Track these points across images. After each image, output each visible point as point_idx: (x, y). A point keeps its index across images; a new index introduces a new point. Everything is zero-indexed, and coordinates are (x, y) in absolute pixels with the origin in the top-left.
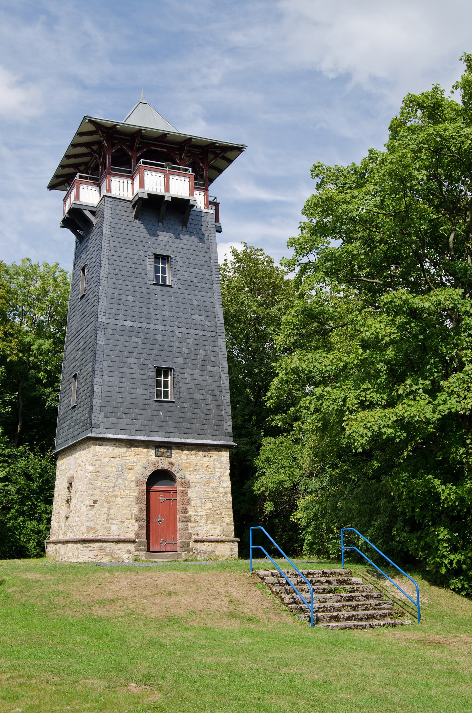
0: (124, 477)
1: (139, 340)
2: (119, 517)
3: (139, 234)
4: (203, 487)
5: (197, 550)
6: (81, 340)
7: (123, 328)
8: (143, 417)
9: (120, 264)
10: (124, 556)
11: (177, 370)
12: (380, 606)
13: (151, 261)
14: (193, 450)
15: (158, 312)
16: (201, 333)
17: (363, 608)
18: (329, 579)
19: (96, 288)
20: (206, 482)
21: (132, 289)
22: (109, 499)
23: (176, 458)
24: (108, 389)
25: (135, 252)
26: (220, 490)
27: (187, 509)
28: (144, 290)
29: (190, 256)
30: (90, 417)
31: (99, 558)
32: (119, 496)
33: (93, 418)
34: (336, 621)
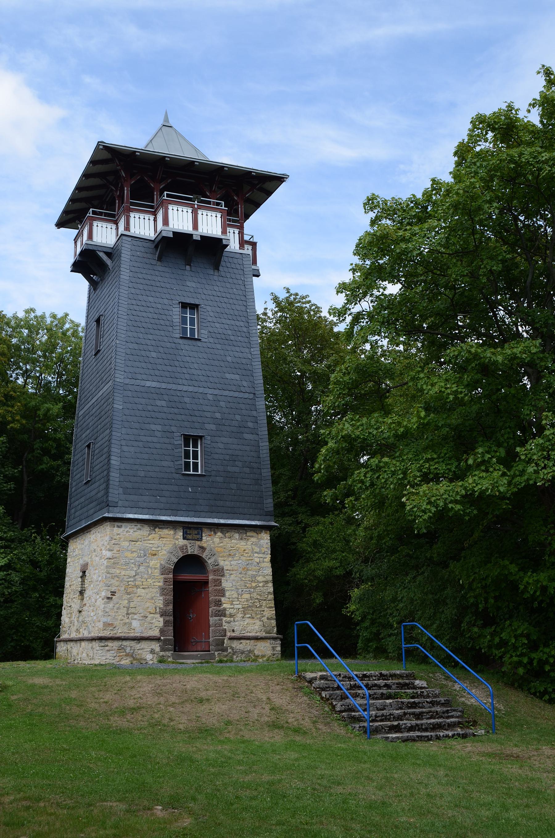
0: (147, 564)
1: (164, 403)
2: (141, 611)
4: (240, 576)
5: (233, 650)
10: (148, 656)
12: (448, 713)
13: (177, 310)
15: (185, 370)
16: (236, 394)
17: (428, 716)
20: (243, 569)
23: (207, 541)
26: (260, 579)
27: (221, 601)
30: (107, 493)
31: (117, 659)
32: (141, 587)
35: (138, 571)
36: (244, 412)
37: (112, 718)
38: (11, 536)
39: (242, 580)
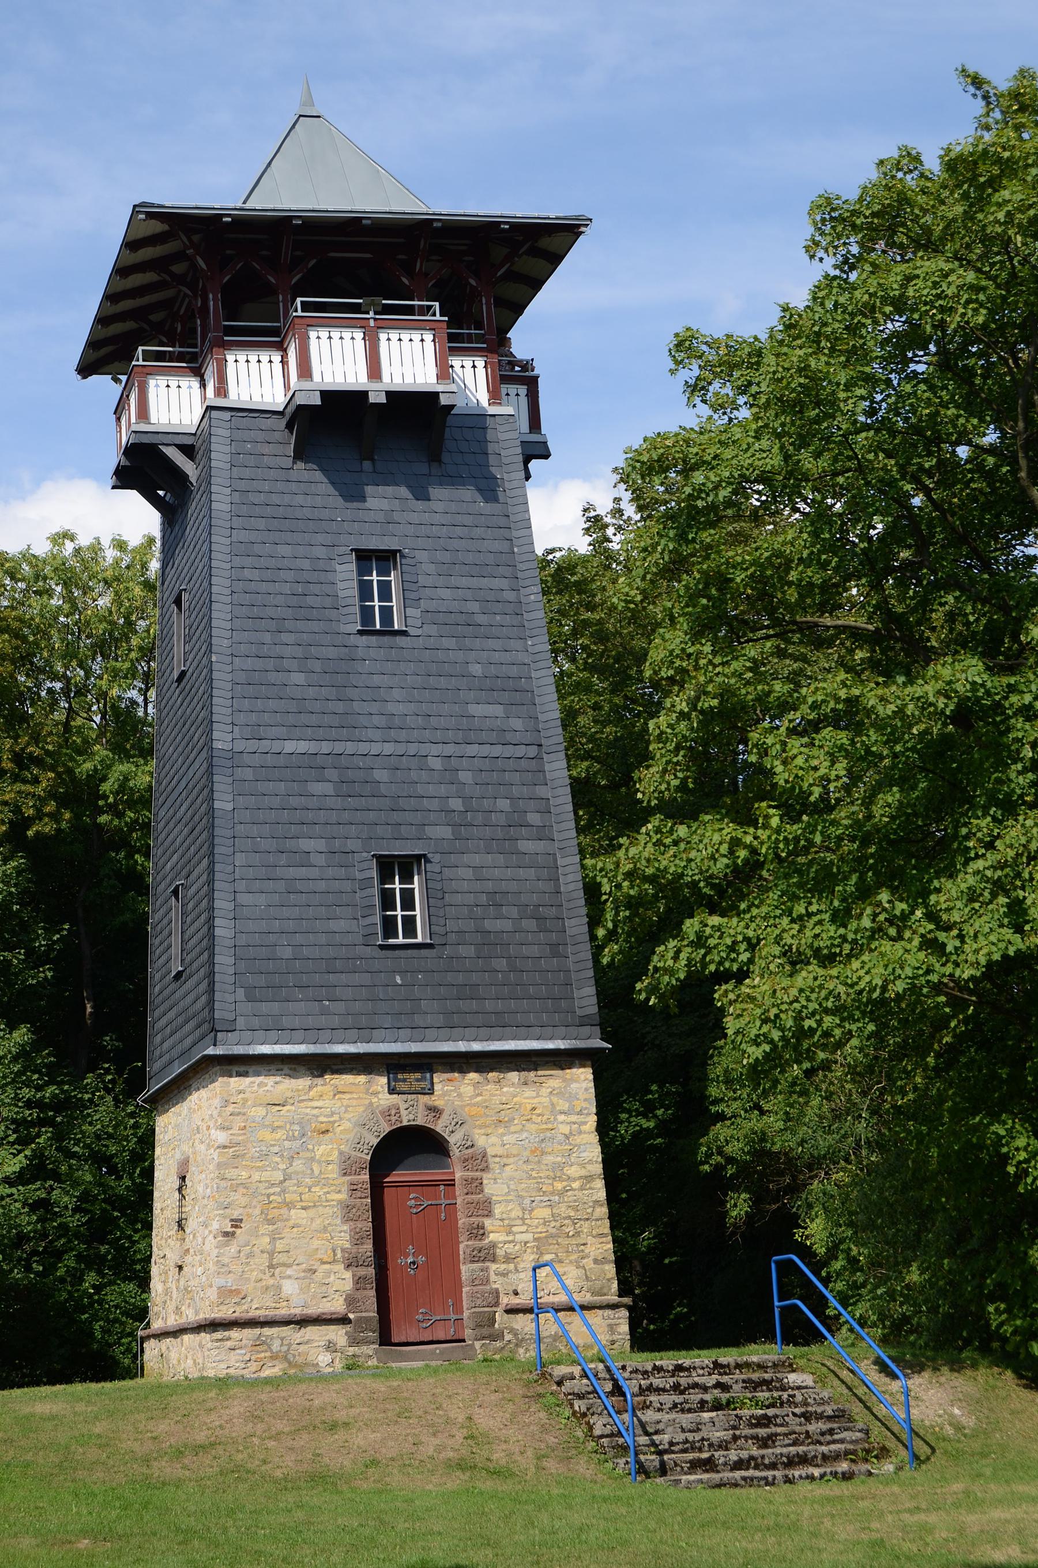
0: (309, 1155)
1: (328, 788)
2: (301, 1259)
3: (309, 501)
4: (525, 1167)
5: (516, 1335)
6: (184, 794)
7: (281, 761)
8: (349, 993)
9: (264, 587)
10: (320, 1358)
11: (435, 858)
12: (832, 1434)
13: (347, 571)
14: (492, 1070)
15: (374, 707)
16: (497, 750)
17: (787, 1442)
18: (725, 1379)
19: (205, 661)
20: (533, 1152)
21: (299, 652)
22: (273, 1213)
23: (444, 1094)
24: (251, 926)
25: (301, 551)
26: (573, 1171)
27: (483, 1228)
28: (332, 652)
29: (456, 544)
31: (254, 1366)
32: (299, 1205)
33: (217, 1005)
34: (707, 1471)
35: (288, 1171)
36: (515, 791)
37: (155, 1464)
38: (54, 1096)
39: (530, 1177)
